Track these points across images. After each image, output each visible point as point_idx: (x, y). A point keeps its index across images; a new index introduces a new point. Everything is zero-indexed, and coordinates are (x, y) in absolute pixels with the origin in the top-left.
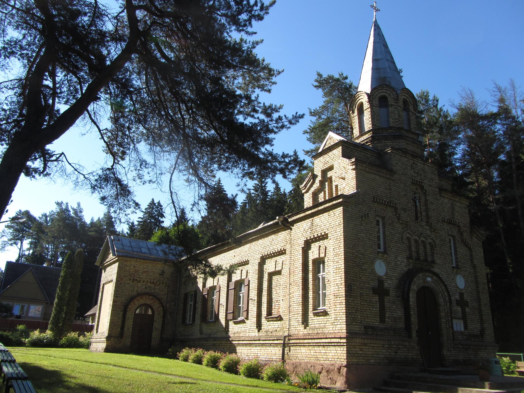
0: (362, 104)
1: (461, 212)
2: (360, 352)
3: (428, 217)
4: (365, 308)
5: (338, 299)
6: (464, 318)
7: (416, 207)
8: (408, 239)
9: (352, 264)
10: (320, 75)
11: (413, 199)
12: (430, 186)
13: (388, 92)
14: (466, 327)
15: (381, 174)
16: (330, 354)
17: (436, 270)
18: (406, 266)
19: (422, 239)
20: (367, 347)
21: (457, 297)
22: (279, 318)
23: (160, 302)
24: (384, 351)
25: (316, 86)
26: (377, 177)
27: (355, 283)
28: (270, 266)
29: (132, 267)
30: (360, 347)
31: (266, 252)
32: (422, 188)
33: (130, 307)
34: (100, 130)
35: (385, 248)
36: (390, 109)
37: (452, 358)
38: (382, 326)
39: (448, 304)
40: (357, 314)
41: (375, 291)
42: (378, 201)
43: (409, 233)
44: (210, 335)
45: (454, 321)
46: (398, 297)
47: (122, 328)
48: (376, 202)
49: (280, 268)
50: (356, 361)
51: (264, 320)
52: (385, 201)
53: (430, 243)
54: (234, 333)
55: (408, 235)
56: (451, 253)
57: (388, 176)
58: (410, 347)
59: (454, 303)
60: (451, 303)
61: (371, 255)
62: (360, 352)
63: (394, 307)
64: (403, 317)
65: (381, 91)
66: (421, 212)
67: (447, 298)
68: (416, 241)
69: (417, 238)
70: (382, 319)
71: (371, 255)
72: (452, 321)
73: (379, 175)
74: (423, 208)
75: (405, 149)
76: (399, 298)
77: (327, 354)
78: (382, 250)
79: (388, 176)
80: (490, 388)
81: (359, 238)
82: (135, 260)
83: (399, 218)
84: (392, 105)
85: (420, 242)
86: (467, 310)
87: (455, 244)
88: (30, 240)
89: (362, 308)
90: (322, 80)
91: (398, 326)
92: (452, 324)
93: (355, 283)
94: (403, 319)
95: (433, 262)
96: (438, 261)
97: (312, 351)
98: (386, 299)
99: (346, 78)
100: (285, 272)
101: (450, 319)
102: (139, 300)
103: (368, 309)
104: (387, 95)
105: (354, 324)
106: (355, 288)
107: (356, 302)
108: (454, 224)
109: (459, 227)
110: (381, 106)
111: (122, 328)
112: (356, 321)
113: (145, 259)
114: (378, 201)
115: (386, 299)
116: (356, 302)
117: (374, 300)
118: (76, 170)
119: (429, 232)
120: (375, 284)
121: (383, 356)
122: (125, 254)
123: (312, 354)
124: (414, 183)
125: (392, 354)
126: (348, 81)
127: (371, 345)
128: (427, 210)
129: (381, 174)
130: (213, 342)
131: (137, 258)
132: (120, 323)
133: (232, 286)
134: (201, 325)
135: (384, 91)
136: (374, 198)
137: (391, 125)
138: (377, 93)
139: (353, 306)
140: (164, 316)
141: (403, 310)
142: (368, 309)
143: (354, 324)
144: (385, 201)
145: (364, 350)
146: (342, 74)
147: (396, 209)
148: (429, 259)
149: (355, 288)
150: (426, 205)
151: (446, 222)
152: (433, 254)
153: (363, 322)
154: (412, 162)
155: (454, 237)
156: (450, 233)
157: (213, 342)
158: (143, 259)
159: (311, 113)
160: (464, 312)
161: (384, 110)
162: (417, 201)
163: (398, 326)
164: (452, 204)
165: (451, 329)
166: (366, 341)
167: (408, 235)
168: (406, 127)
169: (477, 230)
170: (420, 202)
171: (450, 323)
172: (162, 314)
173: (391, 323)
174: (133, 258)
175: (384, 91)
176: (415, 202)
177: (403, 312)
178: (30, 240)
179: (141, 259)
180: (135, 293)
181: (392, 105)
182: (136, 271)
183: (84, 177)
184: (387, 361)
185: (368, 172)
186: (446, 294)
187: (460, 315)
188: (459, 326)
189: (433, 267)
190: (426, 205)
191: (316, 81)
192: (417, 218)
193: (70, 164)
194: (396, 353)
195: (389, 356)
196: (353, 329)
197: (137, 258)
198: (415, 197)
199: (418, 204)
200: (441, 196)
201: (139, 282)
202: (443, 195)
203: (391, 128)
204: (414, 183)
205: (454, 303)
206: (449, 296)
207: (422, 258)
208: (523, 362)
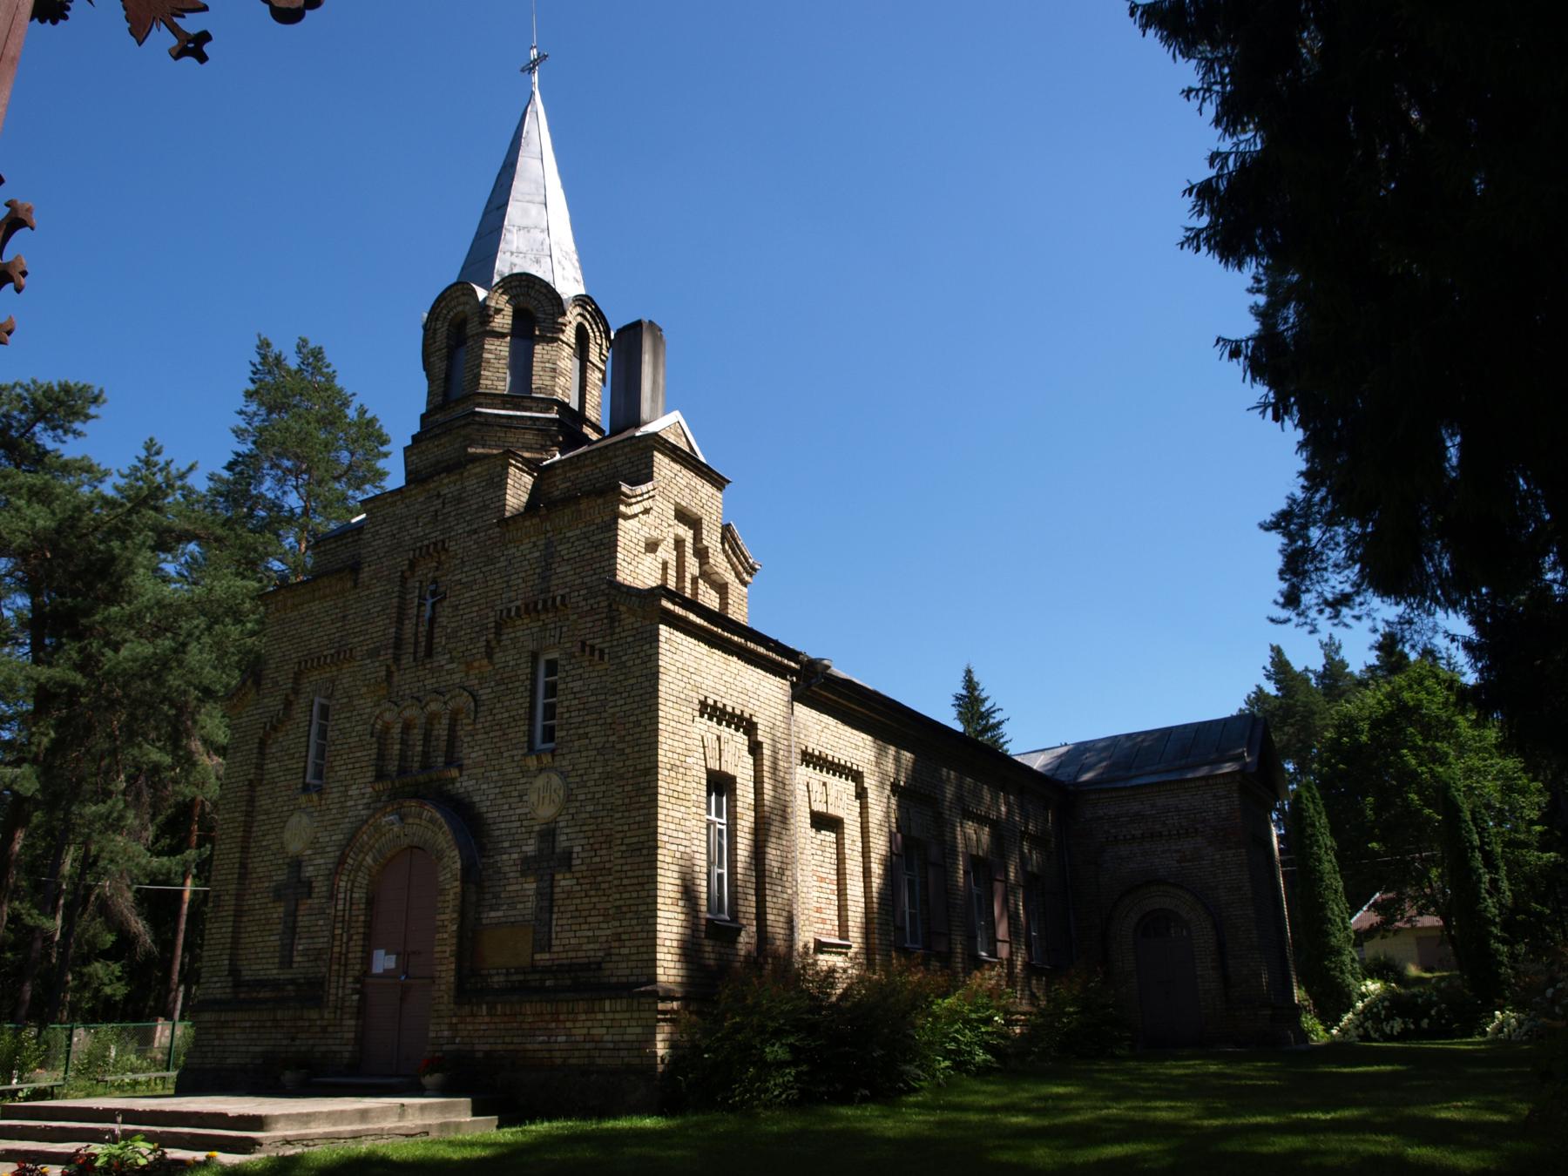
38: (286, 975)
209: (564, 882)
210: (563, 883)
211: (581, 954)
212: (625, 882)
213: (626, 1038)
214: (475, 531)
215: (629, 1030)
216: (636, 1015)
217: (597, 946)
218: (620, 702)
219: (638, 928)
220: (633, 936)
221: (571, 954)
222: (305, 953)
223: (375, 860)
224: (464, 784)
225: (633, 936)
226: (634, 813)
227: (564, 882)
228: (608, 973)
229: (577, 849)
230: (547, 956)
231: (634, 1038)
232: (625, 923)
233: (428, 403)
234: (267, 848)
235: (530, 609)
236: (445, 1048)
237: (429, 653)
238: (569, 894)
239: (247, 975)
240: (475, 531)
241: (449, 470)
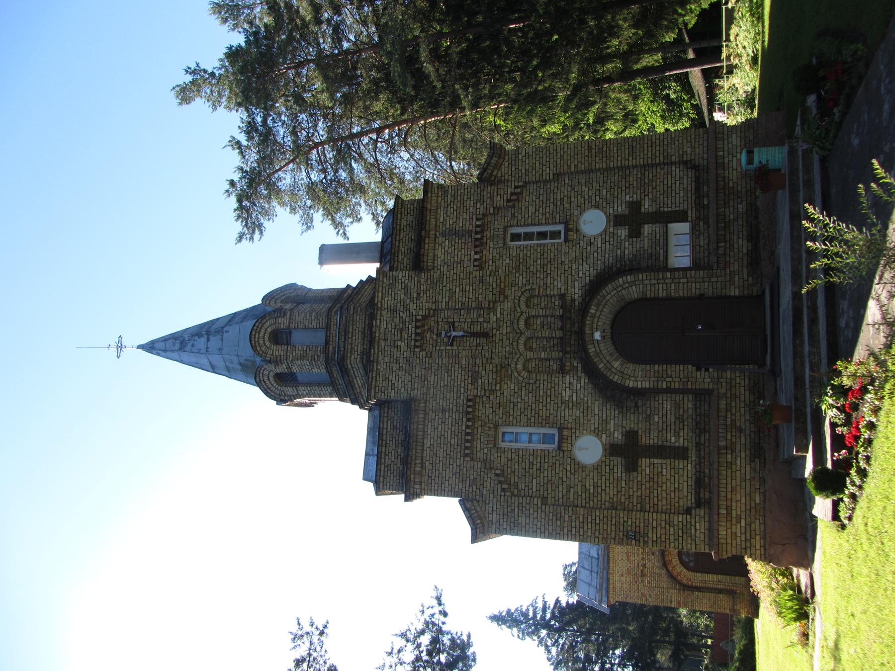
2: (743, 522)
4: (664, 495)
9: (590, 525)
10: (241, 237)
14: (680, 217)
18: (579, 379)
20: (734, 504)
24: (738, 462)
25: (261, 233)
27: (622, 521)
29: (623, 579)
30: (734, 520)
38: (693, 455)
40: (676, 523)
41: (632, 467)
46: (637, 406)
47: (720, 591)
50: (758, 537)
62: (743, 522)
65: (267, 382)
70: (680, 453)
75: (362, 358)
76: (640, 403)
80: (807, 452)
82: (611, 577)
90: (248, 229)
93: (622, 521)
98: (644, 440)
99: (232, 183)
102: (674, 567)
105: (693, 531)
106: (630, 523)
107: (655, 525)
108: (481, 229)
111: (720, 591)
112: (689, 527)
113: (608, 560)
115: (644, 440)
116: (655, 525)
120: (618, 461)
121: (748, 466)
122: (604, 592)
126: (236, 177)
127: (729, 496)
131: (608, 573)
132: (712, 595)
143: (693, 531)
145: (739, 513)
146: (227, 191)
149: (630, 523)
154: (383, 344)
158: (608, 563)
159: (309, 228)
161: (296, 337)
166: (723, 511)
173: (686, 431)
174: (608, 580)
175: (266, 378)
179: (608, 567)
180: (663, 572)
182: (629, 572)
184: (757, 460)
185: (422, 467)
187: (658, 228)
189: (573, 300)
191: (252, 239)
192: (485, 335)
197: (608, 573)
201: (644, 566)
204: (421, 336)
209: (647, 206)
210: (646, 206)
211: (689, 189)
212: (650, 155)
213: (739, 144)
214: (418, 294)
215: (734, 143)
216: (726, 137)
217: (685, 177)
218: (548, 171)
219: (677, 143)
220: (681, 146)
221: (689, 195)
222: (677, 435)
223: (616, 360)
224: (576, 292)
225: (681, 146)
226: (612, 154)
227: (647, 206)
228: (701, 161)
229: (627, 199)
230: (690, 211)
231: (739, 139)
232: (673, 153)
233: (331, 396)
234: (596, 486)
235: (479, 245)
236: (745, 276)
237: (485, 335)
238: (653, 200)
239: (690, 501)
240: (418, 294)
241: (372, 317)
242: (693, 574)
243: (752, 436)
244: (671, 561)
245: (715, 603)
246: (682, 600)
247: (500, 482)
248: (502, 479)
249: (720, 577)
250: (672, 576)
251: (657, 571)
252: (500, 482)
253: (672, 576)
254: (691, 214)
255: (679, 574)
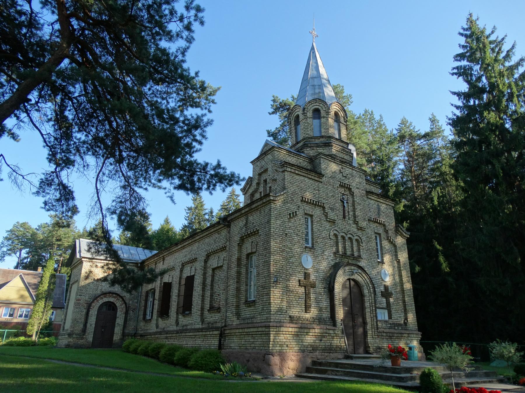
0: (298, 116)
1: (386, 212)
3: (355, 216)
4: (291, 299)
5: (265, 290)
6: (388, 307)
7: (344, 206)
8: (336, 235)
11: (341, 200)
12: (358, 188)
13: (321, 105)
14: (390, 317)
15: (310, 177)
16: (257, 343)
17: (362, 264)
19: (349, 236)
21: (382, 289)
22: (218, 310)
23: (123, 300)
26: (306, 179)
28: (214, 262)
31: (210, 249)
32: (350, 189)
33: (93, 304)
34: (42, 135)
35: (313, 244)
36: (323, 120)
37: (376, 345)
39: (373, 295)
42: (307, 200)
43: (336, 230)
44: (164, 329)
45: (378, 311)
48: (305, 201)
49: (222, 264)
51: (206, 312)
52: (313, 201)
53: (357, 240)
54: (183, 326)
55: (335, 232)
56: (377, 249)
57: (317, 179)
58: (335, 335)
59: (379, 294)
60: (375, 294)
61: (299, 250)
63: (320, 297)
64: (329, 307)
66: (348, 212)
67: (372, 290)
68: (343, 237)
69: (344, 234)
71: (299, 250)
72: (376, 311)
73: (308, 178)
74: (351, 208)
76: (325, 290)
77: (255, 343)
78: (310, 245)
79: (317, 179)
81: (286, 234)
83: (326, 216)
84: (324, 117)
85: (347, 238)
86: (391, 300)
87: (381, 241)
88: (28, 250)
89: (288, 299)
91: (324, 315)
92: (376, 314)
94: (329, 309)
95: (359, 256)
96: (364, 256)
97: (243, 341)
100: (225, 267)
101: (374, 308)
103: (294, 299)
104: (320, 108)
105: (279, 313)
106: (281, 279)
109: (384, 225)
110: (314, 118)
114: (307, 200)
117: (300, 291)
118: (14, 171)
119: (355, 230)
121: (307, 344)
123: (243, 343)
124: (342, 186)
125: (317, 341)
128: (354, 210)
129: (310, 177)
130: (165, 336)
132: (83, 320)
133: (183, 282)
134: (157, 320)
135: (318, 104)
136: (303, 198)
137: (323, 134)
138: (311, 106)
139: (278, 297)
140: (127, 313)
141: (329, 300)
142: (294, 299)
143: (279, 313)
144: (313, 201)
147: (324, 208)
148: (356, 254)
149: (281, 279)
150: (353, 205)
151: (373, 221)
152: (359, 250)
153: (288, 312)
155: (379, 234)
156: (376, 231)
157: (165, 336)
160: (388, 303)
161: (316, 121)
162: (345, 202)
163: (324, 315)
164: (378, 205)
165: (375, 318)
167: (335, 232)
168: (337, 137)
169: (401, 229)
170: (347, 203)
171: (374, 312)
172: (124, 310)
175: (318, 104)
176: (343, 203)
177: (329, 303)
178: (28, 250)
180: (99, 292)
181: (324, 117)
183: (23, 178)
184: (311, 349)
186: (371, 286)
187: (385, 305)
188: (383, 315)
189: (359, 261)
190: (353, 205)
192: (344, 217)
193: (8, 166)
194: (321, 340)
195: (313, 344)
196: (277, 318)
198: (343, 198)
199: (346, 205)
200: (368, 198)
202: (369, 197)
203: (322, 137)
205: (379, 294)
206: (374, 288)
207: (349, 253)
208: (1, 270)
242: (97, 309)
243: (321, 346)
244: (105, 297)
245: (77, 322)
246: (81, 302)
247: (293, 213)
248: (294, 214)
249: (94, 326)
250: (96, 298)
251: (100, 288)
252: (293, 213)
253: (96, 298)
254: (391, 321)
255: (98, 301)
